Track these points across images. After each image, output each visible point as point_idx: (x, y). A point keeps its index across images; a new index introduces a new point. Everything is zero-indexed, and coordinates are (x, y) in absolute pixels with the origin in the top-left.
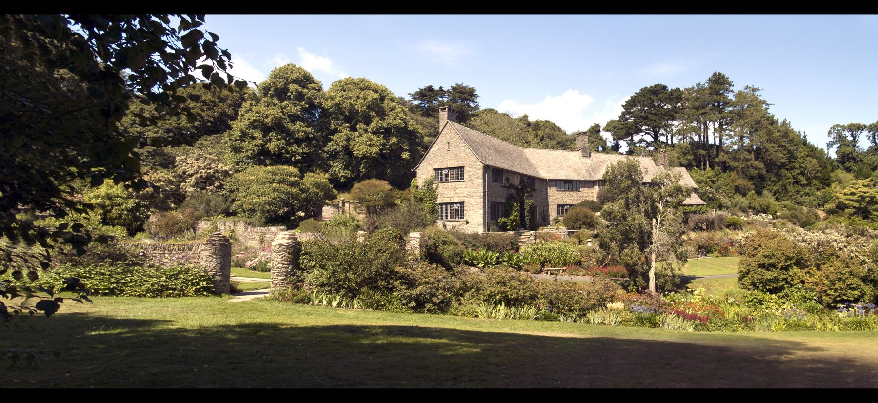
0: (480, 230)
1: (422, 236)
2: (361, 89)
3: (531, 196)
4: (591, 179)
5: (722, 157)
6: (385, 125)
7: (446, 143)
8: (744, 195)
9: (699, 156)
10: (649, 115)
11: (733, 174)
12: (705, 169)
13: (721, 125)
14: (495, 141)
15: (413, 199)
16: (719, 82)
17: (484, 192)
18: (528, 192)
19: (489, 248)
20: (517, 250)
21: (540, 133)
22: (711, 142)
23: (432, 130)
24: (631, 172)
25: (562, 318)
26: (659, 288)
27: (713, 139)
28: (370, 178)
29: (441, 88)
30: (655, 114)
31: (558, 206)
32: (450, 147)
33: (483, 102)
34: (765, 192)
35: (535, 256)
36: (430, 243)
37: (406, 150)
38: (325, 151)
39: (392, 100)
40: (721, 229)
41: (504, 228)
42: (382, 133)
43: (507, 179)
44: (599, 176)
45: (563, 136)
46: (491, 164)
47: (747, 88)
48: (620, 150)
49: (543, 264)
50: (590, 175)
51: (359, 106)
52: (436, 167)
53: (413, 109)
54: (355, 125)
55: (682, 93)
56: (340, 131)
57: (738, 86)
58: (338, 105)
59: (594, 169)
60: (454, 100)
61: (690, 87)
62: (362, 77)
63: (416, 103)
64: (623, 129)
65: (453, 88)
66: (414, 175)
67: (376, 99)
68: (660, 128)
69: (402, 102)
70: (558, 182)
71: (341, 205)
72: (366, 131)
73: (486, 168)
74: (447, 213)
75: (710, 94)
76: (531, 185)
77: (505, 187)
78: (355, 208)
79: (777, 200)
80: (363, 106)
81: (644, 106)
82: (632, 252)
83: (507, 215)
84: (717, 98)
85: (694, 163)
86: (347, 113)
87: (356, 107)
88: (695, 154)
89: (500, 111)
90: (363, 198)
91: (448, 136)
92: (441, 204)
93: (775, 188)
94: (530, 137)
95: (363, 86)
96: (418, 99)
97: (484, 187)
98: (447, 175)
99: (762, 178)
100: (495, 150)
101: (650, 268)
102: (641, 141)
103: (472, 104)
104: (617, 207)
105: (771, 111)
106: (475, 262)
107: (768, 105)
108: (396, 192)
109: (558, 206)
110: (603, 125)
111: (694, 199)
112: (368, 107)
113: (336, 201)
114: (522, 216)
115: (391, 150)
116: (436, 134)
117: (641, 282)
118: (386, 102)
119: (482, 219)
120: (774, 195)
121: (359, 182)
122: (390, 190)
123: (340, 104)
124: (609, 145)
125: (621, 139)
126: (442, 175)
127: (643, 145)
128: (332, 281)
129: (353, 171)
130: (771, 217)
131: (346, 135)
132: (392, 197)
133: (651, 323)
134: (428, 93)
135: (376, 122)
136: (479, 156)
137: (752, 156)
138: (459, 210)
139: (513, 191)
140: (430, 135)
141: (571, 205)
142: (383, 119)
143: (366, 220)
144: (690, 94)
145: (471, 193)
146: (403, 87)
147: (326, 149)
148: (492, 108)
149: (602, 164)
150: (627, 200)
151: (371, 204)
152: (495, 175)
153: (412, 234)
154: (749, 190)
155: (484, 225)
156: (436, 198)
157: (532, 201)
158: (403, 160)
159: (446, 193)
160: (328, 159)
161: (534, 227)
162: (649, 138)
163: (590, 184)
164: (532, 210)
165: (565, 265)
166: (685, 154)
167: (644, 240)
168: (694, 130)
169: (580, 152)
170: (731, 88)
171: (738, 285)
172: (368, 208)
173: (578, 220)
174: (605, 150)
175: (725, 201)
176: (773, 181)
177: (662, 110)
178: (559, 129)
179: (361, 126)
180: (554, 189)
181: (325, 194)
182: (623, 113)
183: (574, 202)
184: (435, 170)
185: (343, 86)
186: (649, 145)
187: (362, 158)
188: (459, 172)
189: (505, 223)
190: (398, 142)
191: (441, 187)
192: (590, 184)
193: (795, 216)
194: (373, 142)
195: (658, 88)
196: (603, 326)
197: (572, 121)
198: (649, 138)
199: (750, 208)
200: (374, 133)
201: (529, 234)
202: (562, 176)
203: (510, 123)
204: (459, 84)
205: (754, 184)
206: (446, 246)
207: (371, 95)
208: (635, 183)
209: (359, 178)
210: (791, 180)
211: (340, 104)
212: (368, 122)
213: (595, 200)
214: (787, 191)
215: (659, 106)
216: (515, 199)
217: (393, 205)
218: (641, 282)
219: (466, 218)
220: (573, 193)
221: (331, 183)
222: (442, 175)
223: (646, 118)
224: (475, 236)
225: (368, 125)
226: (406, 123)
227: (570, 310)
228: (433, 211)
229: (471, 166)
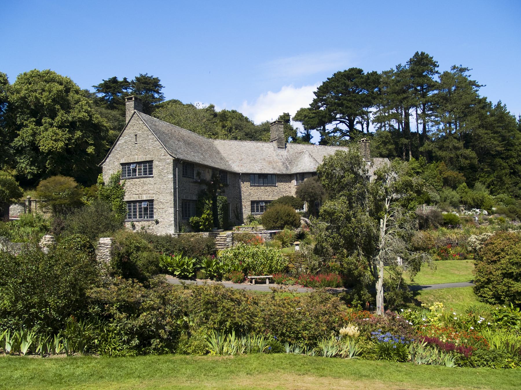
0: (171, 231)
1: (114, 242)
2: (46, 81)
3: (224, 192)
4: (288, 172)
5: (427, 146)
6: (70, 119)
7: (133, 135)
8: (454, 188)
9: (400, 145)
10: (345, 102)
11: (442, 165)
12: (408, 160)
14: (185, 132)
15: (99, 197)
16: (422, 63)
17: (175, 189)
18: (220, 188)
19: (185, 253)
20: (215, 253)
21: (228, 124)
23: (116, 124)
25: (288, 349)
26: (388, 303)
27: (415, 126)
28: (55, 175)
29: (125, 79)
30: (350, 101)
31: (253, 202)
32: (137, 140)
33: (168, 93)
34: (478, 184)
35: (237, 262)
36: (123, 250)
37: (91, 144)
38: (12, 147)
39: (77, 92)
40: (437, 228)
41: (196, 228)
42: (67, 127)
43: (199, 174)
45: (252, 127)
46: (181, 157)
47: (454, 68)
48: (312, 141)
49: (246, 271)
50: (287, 168)
51: (45, 99)
53: (98, 102)
54: (41, 119)
55: (380, 76)
56: (26, 126)
57: (444, 66)
58: (24, 99)
59: (290, 161)
60: (137, 91)
61: (389, 69)
62: (47, 68)
63: (100, 95)
64: (313, 118)
65: (137, 79)
66: (100, 171)
67: (61, 91)
68: (356, 115)
69: (87, 94)
70: (252, 176)
71: (27, 203)
72: (51, 125)
73: (177, 162)
74: (135, 212)
75: (412, 76)
76: (224, 181)
77: (196, 182)
78: (41, 207)
79: (492, 193)
80: (48, 99)
81: (338, 92)
82: (356, 259)
83: (199, 214)
84: (420, 80)
85: (395, 153)
86: (32, 107)
87: (41, 101)
88: (396, 143)
89: (185, 102)
90: (50, 196)
91: (135, 127)
92: (129, 202)
93: (489, 180)
94: (218, 129)
95: (49, 78)
96: (102, 91)
97: (175, 183)
98: (134, 170)
99: (473, 168)
100: (185, 141)
101: (377, 278)
102: (336, 130)
103: (156, 96)
105: (482, 93)
106: (170, 269)
107: (478, 86)
108: (83, 190)
109: (253, 202)
110: (293, 114)
112: (54, 100)
113: (22, 199)
114: (215, 214)
115: (76, 145)
116: (121, 128)
117: (366, 295)
118: (71, 94)
119: (173, 219)
120: (488, 187)
121: (45, 179)
122: (76, 187)
123: (25, 97)
124: (299, 135)
125: (313, 128)
126: (130, 169)
127: (338, 134)
128: (20, 306)
129: (39, 167)
130: (486, 212)
131: (32, 129)
132: (78, 194)
133: (399, 356)
134: (113, 85)
135: (61, 116)
136: (169, 149)
137: (461, 144)
138: (147, 209)
139: (204, 187)
140: (114, 129)
141: (266, 202)
142: (68, 112)
143: (52, 220)
144: (389, 77)
145: (160, 189)
146: (87, 79)
147: (12, 145)
148: (176, 98)
149: (310, 158)
150: (350, 200)
151: (57, 202)
152: (186, 170)
153: (102, 240)
154: (460, 183)
155: (176, 225)
156: (123, 195)
157: (225, 198)
158: (88, 154)
159: (135, 190)
160: (15, 154)
161: (228, 228)
162: (344, 127)
163: (287, 178)
164: (226, 208)
165: (270, 272)
166: (385, 143)
167: (370, 249)
169: (275, 144)
170: (436, 69)
171: (475, 297)
172: (54, 206)
173: (278, 218)
174: (295, 140)
175: (434, 195)
176: (487, 172)
177: (358, 97)
178: (246, 119)
179: (46, 120)
180: (248, 184)
181: (11, 192)
183: (270, 198)
184: (122, 164)
185: (29, 79)
187: (48, 154)
188: (146, 167)
189: (197, 223)
190: (83, 136)
191: (128, 183)
192: (287, 178)
193: (514, 212)
194: (58, 137)
195: (353, 72)
196: (338, 360)
197: (260, 115)
198: (344, 127)
199: (461, 202)
200: (59, 127)
201: (224, 235)
202: (256, 169)
203: (196, 114)
204: (144, 74)
205: (464, 175)
206: (139, 253)
207: (57, 87)
209: (43, 175)
210: (507, 171)
211: (25, 97)
212: (53, 116)
213: (295, 196)
214: (503, 183)
215: (354, 92)
216: (207, 195)
217: (80, 205)
218: (366, 295)
219: (155, 217)
220: (268, 189)
221: (17, 181)
222: (129, 170)
223: (339, 105)
224: (168, 238)
225: (53, 119)
226: (91, 116)
227: (297, 338)
228: (121, 209)
229: (160, 160)
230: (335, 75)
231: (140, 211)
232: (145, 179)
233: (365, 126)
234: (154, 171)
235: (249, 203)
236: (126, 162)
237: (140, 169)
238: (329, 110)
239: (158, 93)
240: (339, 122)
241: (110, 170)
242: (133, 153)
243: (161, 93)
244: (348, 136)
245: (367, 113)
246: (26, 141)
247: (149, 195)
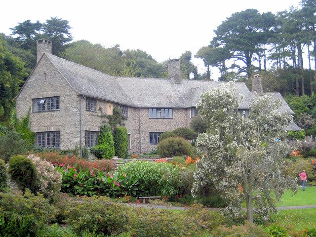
53: (11, 42)
63: (17, 36)
65: (48, 21)
102: (233, 66)
103: (65, 36)
110: (194, 52)
127: (236, 70)
230: (233, 15)
231: (49, 141)
232: (53, 113)
234: (61, 106)
235: (148, 135)
236: (37, 98)
237: (49, 104)
238: (228, 48)
239: (66, 32)
240: (237, 59)
241: (22, 104)
242: (43, 90)
243: (69, 34)
244: (245, 71)
245: (262, 50)
247: (56, 127)
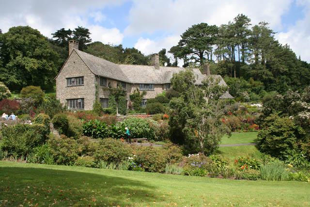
13: (243, 47)
22: (237, 59)
24: (188, 79)
32: (78, 62)
44: (168, 81)
47: (260, 23)
52: (67, 77)
63: (55, 39)
102: (192, 58)
103: (87, 39)
104: (178, 100)
110: (168, 49)
111: (227, 96)
127: (194, 61)
168: (226, 51)
170: (250, 23)
174: (169, 65)
182: (181, 41)
186: (197, 61)
197: (146, 48)
208: (189, 84)
233: (210, 56)
239: (88, 36)
246: (22, 63)
